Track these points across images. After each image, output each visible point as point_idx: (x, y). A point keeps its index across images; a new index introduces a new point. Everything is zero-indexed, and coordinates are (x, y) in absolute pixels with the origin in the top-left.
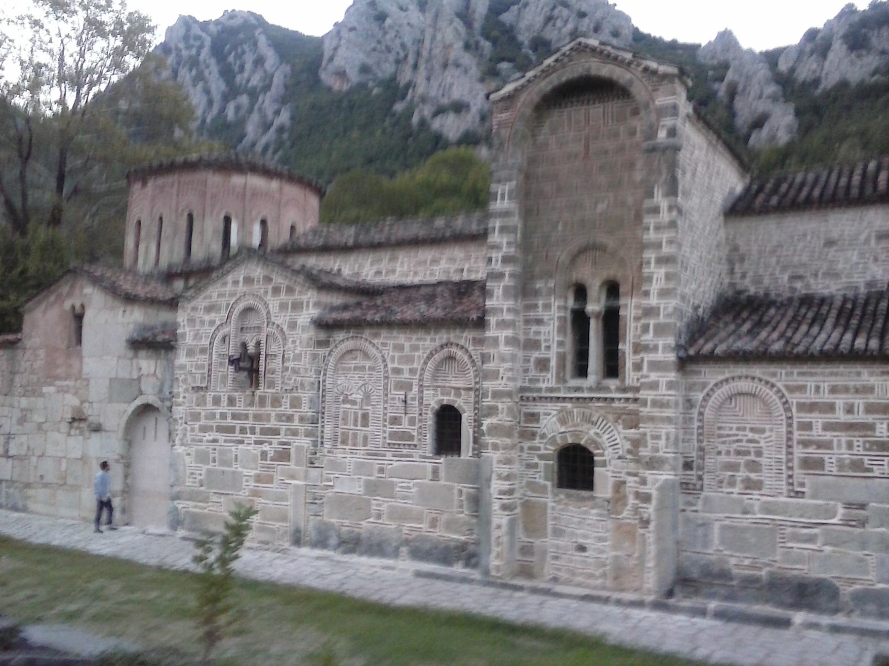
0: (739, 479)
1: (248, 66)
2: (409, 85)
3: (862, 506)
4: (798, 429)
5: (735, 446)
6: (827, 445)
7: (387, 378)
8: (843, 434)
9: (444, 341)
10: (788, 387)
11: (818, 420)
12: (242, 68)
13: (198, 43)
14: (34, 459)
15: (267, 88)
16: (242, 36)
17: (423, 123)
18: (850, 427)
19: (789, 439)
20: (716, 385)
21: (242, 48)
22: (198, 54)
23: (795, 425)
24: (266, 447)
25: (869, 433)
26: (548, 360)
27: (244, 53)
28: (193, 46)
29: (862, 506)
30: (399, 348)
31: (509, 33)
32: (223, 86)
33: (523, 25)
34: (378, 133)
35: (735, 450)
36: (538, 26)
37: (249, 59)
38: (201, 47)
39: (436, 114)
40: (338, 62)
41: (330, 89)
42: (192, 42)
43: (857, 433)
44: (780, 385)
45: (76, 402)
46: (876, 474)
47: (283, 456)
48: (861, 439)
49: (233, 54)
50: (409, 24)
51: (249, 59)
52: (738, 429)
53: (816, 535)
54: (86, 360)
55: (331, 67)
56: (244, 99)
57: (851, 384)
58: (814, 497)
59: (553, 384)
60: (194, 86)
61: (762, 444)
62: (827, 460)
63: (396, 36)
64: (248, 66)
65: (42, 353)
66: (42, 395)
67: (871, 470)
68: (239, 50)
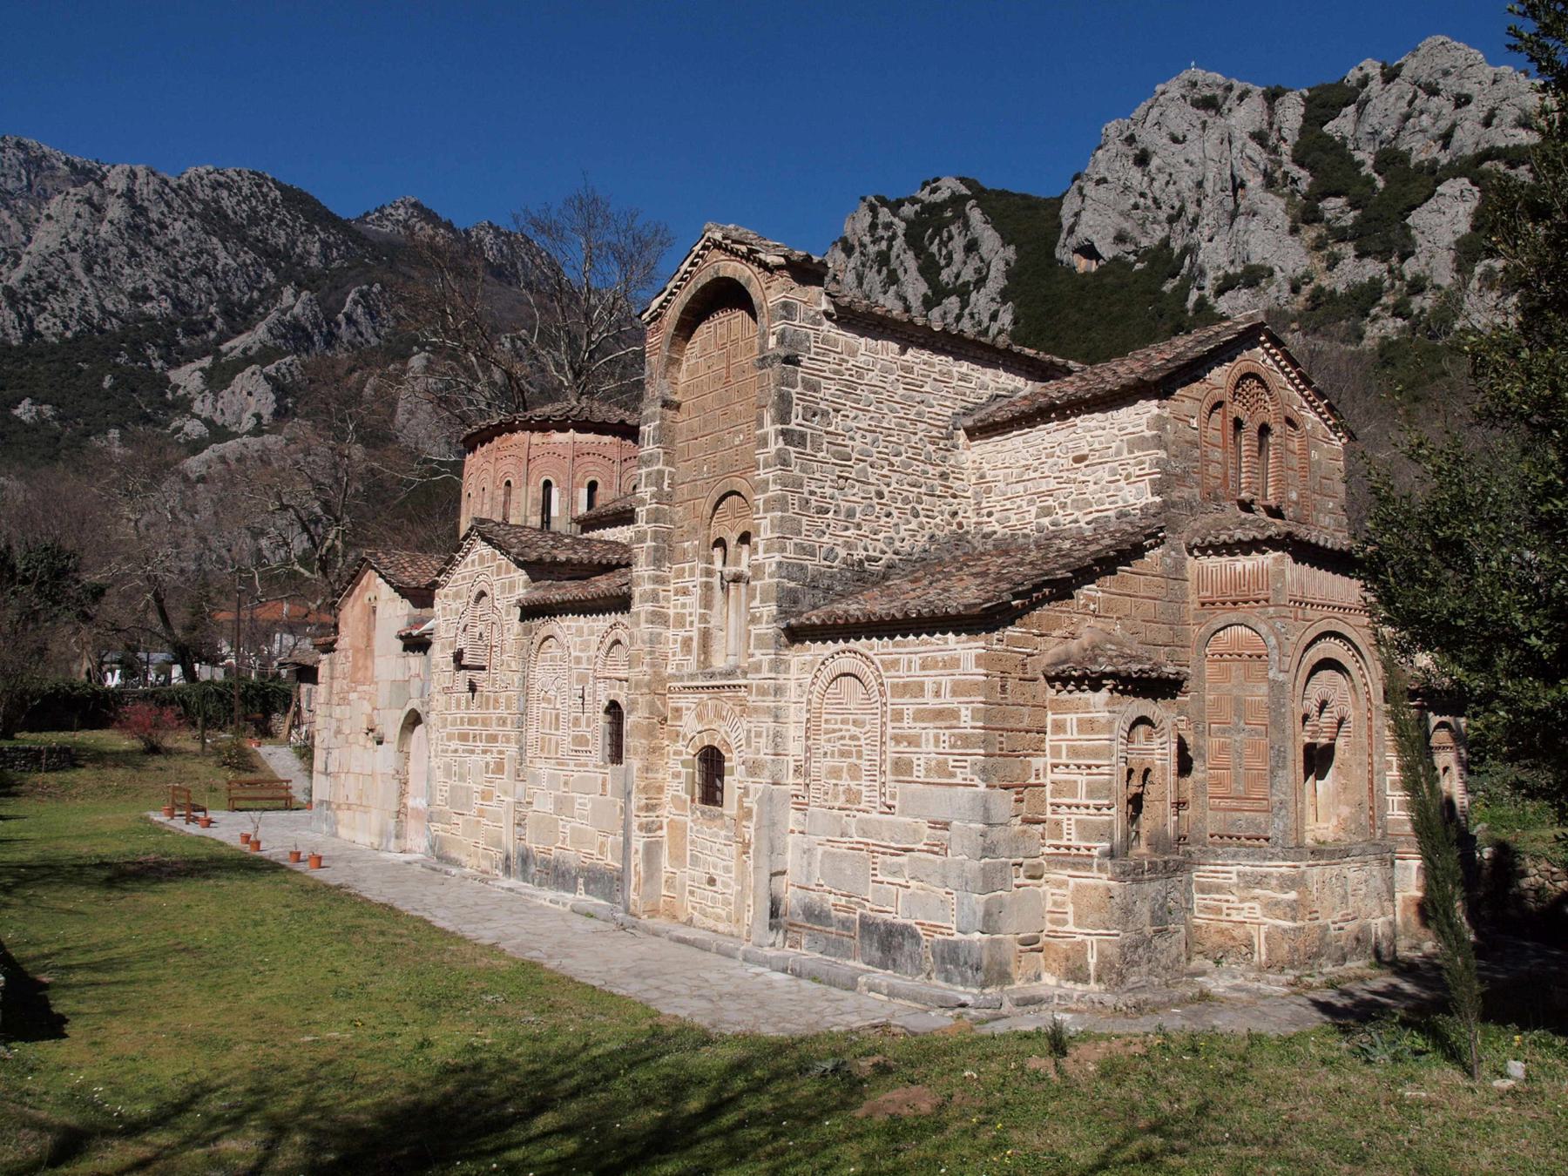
1: (958, 256)
4: (1079, 720)
8: (931, 725)
9: (613, 621)
10: (882, 662)
11: (909, 705)
12: (949, 257)
13: (887, 234)
14: (343, 776)
15: (981, 282)
16: (949, 214)
18: (939, 714)
21: (949, 232)
22: (890, 247)
24: (488, 757)
25: (954, 723)
26: (691, 639)
27: (951, 238)
28: (882, 238)
29: (946, 826)
30: (580, 632)
31: (1338, 150)
32: (923, 288)
35: (839, 750)
36: (1388, 132)
37: (958, 243)
38: (893, 237)
39: (1220, 292)
40: (1083, 232)
42: (881, 232)
43: (943, 724)
44: (876, 659)
46: (958, 780)
47: (500, 768)
48: (947, 732)
49: (937, 241)
50: (1187, 161)
51: (958, 243)
53: (901, 866)
54: (377, 661)
55: (1072, 242)
56: (953, 303)
58: (902, 813)
60: (885, 293)
61: (862, 742)
62: (916, 762)
63: (1168, 183)
64: (958, 256)
65: (350, 653)
67: (953, 775)
68: (945, 234)
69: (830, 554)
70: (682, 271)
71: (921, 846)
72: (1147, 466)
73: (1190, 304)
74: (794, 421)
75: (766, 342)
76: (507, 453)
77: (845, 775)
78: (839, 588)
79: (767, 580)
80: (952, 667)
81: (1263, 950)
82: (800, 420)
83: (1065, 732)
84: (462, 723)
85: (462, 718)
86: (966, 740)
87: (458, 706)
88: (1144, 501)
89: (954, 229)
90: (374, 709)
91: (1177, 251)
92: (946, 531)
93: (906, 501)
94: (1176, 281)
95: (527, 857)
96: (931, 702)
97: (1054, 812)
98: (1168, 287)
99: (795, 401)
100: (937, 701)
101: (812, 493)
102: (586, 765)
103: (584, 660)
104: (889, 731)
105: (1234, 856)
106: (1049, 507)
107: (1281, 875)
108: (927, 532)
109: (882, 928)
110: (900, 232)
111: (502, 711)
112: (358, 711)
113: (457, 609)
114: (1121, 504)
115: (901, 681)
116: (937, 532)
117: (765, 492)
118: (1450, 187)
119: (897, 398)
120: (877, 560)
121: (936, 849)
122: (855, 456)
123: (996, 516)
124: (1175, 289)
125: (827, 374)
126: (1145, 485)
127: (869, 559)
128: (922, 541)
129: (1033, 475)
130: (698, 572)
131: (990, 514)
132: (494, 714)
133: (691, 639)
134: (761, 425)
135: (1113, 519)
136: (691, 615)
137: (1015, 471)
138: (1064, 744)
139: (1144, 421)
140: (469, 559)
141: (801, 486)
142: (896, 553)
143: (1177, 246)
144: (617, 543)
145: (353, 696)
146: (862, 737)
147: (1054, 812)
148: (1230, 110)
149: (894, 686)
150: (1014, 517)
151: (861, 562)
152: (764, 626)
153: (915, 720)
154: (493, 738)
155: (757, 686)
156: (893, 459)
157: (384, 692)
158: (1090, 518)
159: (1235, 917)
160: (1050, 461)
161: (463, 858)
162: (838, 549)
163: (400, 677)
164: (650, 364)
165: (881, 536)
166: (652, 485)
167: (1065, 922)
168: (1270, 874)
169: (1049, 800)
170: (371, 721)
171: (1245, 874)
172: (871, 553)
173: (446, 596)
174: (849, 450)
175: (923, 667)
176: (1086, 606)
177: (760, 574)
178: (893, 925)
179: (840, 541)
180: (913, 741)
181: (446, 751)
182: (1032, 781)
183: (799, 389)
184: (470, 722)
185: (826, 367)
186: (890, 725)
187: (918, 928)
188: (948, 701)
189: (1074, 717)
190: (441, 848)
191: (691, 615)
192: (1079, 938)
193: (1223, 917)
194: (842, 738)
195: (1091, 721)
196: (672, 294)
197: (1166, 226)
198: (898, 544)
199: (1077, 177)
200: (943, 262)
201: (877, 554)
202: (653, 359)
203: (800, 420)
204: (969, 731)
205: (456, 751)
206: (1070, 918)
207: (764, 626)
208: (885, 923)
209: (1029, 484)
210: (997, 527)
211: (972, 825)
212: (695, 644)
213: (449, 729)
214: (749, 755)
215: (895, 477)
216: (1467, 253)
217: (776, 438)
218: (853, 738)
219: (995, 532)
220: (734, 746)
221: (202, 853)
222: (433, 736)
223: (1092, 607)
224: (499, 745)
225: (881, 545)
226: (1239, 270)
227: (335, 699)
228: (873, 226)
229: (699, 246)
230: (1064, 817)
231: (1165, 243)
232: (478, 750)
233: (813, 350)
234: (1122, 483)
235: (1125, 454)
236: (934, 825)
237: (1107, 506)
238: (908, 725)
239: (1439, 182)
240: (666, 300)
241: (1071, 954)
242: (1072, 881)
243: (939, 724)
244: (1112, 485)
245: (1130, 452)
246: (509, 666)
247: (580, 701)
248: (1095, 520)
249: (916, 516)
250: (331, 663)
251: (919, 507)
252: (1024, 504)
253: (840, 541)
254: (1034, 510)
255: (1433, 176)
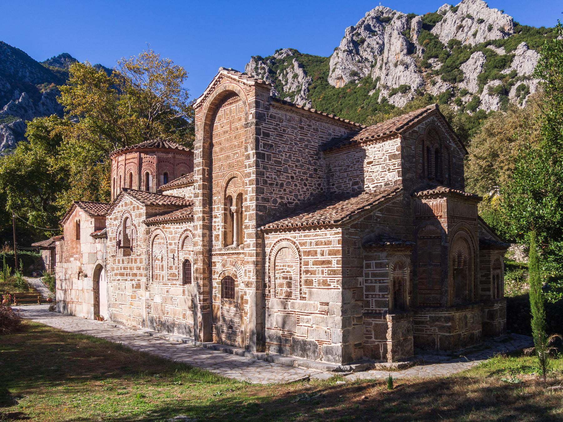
0: (284, 291)
1: (290, 80)
2: (378, 79)
3: (327, 304)
4: (376, 263)
5: (282, 275)
6: (313, 273)
7: (167, 248)
8: (320, 266)
10: (300, 243)
11: (311, 259)
12: (287, 82)
13: (262, 72)
17: (384, 100)
18: (323, 263)
19: (300, 271)
20: (275, 244)
21: (286, 71)
23: (302, 263)
24: (133, 282)
25: (330, 265)
26: (219, 235)
27: (287, 73)
28: (260, 73)
33: (443, 34)
34: (359, 109)
37: (290, 76)
41: (334, 87)
42: (259, 71)
43: (325, 266)
44: (297, 242)
45: (79, 265)
46: (332, 287)
47: (138, 286)
49: (281, 75)
51: (290, 76)
52: (283, 266)
54: (82, 245)
57: (323, 240)
59: (220, 247)
61: (292, 273)
62: (314, 281)
66: (70, 262)
67: (329, 285)
69: (275, 201)
70: (210, 87)
71: (317, 312)
72: (396, 165)
73: (379, 101)
74: (260, 149)
75: (248, 117)
76: (130, 161)
77: (285, 286)
78: (278, 215)
79: (251, 212)
80: (328, 245)
81: (439, 344)
82: (262, 149)
83: (371, 268)
84: (121, 269)
85: (121, 267)
86: (334, 272)
87: (119, 263)
88: (395, 179)
89: (288, 70)
90: (82, 264)
91: (374, 79)
92: (317, 192)
93: (302, 180)
94: (374, 91)
95: (152, 320)
96: (320, 258)
97: (366, 297)
98: (371, 93)
99: (260, 141)
100: (323, 257)
101: (267, 177)
102: (176, 284)
103: (173, 244)
104: (303, 269)
105: (428, 311)
106: (357, 182)
107: (446, 317)
108: (310, 192)
109: (302, 343)
110: (267, 71)
111: (138, 264)
112: (74, 266)
113: (116, 224)
114: (386, 180)
115: (308, 250)
116: (313, 192)
117: (249, 177)
118: (476, 55)
119: (298, 140)
120: (292, 203)
121: (323, 313)
122: (283, 162)
123: (336, 185)
124: (374, 94)
125: (272, 130)
126: (395, 173)
127: (289, 203)
128: (308, 195)
129: (350, 169)
130: (220, 209)
131: (333, 185)
132: (134, 265)
133: (219, 235)
134: (247, 151)
135: (383, 186)
136: (218, 226)
137: (343, 168)
138: (370, 272)
139: (395, 148)
140: (120, 204)
141: (263, 175)
142: (299, 200)
143: (374, 77)
144: (179, 197)
145: (72, 259)
146: (292, 271)
147: (366, 297)
148: (395, 23)
149: (305, 252)
150: (343, 186)
151: (286, 204)
152: (251, 230)
153: (313, 265)
154: (135, 275)
155: (249, 253)
156: (297, 164)
157: (85, 259)
158: (374, 185)
159: (428, 333)
160: (357, 164)
161: (124, 321)
162: (278, 199)
163: (92, 251)
164: (197, 125)
165: (293, 194)
166: (200, 175)
167: (371, 338)
168: (442, 317)
169: (365, 293)
170: (80, 268)
171: (432, 317)
172: (290, 201)
173: (111, 219)
174: (280, 160)
175: (317, 245)
176: (376, 220)
177: (248, 210)
178: (306, 341)
179: (278, 196)
180: (313, 273)
181: (115, 280)
182: (359, 286)
183: (262, 136)
184: (124, 269)
185: (271, 127)
186: (303, 267)
187: (317, 342)
188: (327, 258)
189: (374, 262)
190: (114, 318)
191: (218, 226)
192: (376, 343)
193: (425, 333)
194: (284, 272)
195: (381, 263)
196: (206, 97)
197: (370, 68)
198: (299, 197)
199: (336, 49)
200: (284, 83)
201: (292, 201)
202: (198, 123)
203: (262, 149)
204: (336, 268)
205: (119, 280)
206: (373, 337)
207: (251, 230)
208: (303, 341)
209: (349, 173)
210: (336, 190)
211: (337, 304)
212: (220, 237)
213: (116, 272)
214: (246, 279)
215: (298, 170)
216: (483, 80)
217: (253, 156)
218: (287, 272)
219: (335, 192)
220: (238, 276)
221: (36, 324)
222: (109, 274)
223: (378, 220)
224: (138, 278)
225: (293, 197)
226: (397, 87)
227: (64, 260)
228: (256, 68)
229: (217, 77)
230: (370, 299)
231: (370, 76)
232: (129, 279)
233: (267, 120)
234: (387, 172)
235: (388, 161)
236: (322, 304)
237: (381, 181)
238: (311, 267)
239: (472, 53)
240: (203, 100)
241: (373, 349)
242: (373, 322)
243: (323, 266)
244: (383, 173)
245: (390, 160)
246: (141, 246)
247: (172, 260)
248: (377, 186)
249: (306, 185)
250: (61, 246)
251: (307, 182)
252: (347, 181)
253: (278, 196)
254: (351, 183)
255: (473, 50)
